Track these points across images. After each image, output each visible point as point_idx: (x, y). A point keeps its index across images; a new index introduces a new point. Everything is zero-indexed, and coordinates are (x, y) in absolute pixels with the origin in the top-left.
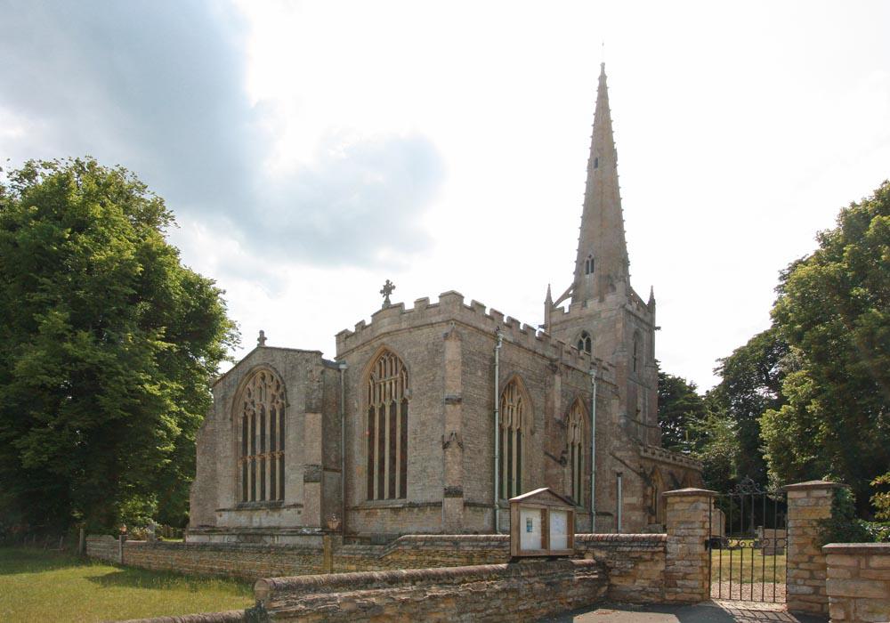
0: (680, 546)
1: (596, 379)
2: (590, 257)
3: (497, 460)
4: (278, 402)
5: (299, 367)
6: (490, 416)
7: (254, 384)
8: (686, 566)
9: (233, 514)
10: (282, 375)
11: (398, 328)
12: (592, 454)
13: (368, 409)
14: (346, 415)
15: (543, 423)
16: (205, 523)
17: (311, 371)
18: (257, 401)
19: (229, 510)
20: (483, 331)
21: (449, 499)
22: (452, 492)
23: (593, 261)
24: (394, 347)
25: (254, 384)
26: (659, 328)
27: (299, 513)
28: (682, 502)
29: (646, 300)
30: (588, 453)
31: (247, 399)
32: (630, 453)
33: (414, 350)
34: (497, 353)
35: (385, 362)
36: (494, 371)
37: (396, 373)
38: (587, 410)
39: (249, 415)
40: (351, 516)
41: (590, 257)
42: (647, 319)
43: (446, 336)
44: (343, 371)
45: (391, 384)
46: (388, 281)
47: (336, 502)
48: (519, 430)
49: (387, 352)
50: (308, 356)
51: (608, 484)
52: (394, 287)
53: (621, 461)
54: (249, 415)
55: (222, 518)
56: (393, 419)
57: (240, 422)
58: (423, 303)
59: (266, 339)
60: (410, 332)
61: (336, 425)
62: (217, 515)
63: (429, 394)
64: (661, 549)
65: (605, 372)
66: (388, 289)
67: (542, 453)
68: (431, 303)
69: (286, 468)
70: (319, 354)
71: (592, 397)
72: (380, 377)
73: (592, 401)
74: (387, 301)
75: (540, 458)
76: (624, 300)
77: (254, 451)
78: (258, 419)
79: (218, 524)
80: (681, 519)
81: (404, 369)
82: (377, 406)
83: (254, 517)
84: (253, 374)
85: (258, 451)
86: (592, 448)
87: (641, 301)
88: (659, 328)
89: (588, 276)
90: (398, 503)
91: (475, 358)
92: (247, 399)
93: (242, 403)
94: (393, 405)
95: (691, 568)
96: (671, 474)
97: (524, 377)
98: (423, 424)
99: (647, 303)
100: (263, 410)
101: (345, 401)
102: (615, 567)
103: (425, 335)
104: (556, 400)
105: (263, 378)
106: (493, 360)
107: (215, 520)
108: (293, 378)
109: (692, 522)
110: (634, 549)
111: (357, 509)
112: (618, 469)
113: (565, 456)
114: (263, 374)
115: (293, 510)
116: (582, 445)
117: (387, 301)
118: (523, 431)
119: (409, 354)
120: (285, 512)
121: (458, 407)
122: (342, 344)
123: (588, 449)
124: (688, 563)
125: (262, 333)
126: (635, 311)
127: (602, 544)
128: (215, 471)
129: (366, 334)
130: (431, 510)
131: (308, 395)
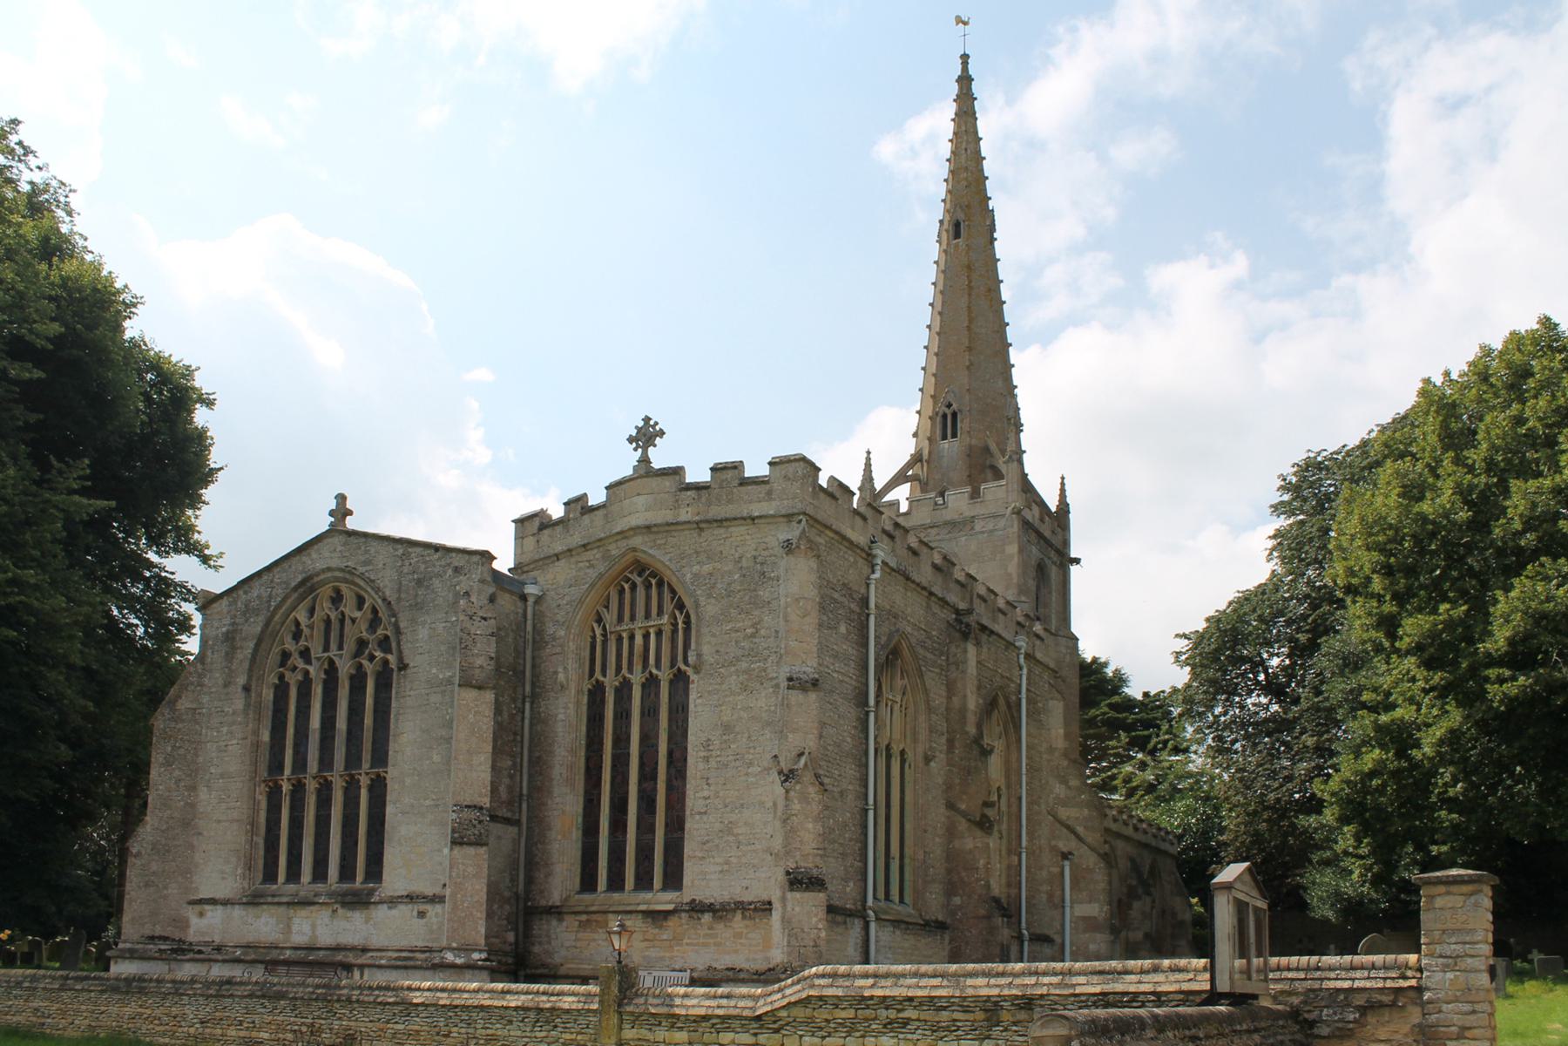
0: (1450, 975)
1: (1028, 656)
2: (949, 405)
3: (871, 814)
4: (372, 658)
5: (436, 583)
6: (859, 719)
7: (312, 611)
8: (1466, 1014)
9: (237, 912)
10: (392, 598)
11: (670, 519)
12: (1020, 811)
13: (587, 686)
14: (534, 697)
15: (943, 740)
16: (158, 931)
17: (467, 594)
18: (316, 651)
19: (225, 903)
20: (851, 542)
21: (798, 895)
22: (799, 881)
23: (954, 415)
24: (661, 555)
25: (312, 611)
26: (1077, 561)
27: (422, 914)
28: (1448, 893)
29: (1053, 504)
30: (1014, 809)
31: (290, 645)
32: (1086, 812)
33: (707, 568)
34: (872, 587)
35: (634, 587)
36: (867, 627)
37: (660, 613)
38: (1012, 717)
39: (293, 679)
40: (541, 927)
41: (949, 405)
42: (1056, 541)
43: (788, 547)
44: (531, 600)
45: (646, 636)
46: (647, 419)
47: (507, 894)
48: (903, 753)
49: (641, 568)
50: (458, 561)
51: (1044, 873)
52: (661, 433)
53: (1068, 827)
54: (293, 679)
55: (204, 922)
56: (650, 712)
57: (268, 695)
58: (727, 472)
59: (350, 513)
60: (701, 530)
61: (512, 716)
62: (191, 914)
63: (744, 665)
64: (1413, 982)
65: (1038, 642)
66: (646, 435)
67: (942, 809)
68: (747, 475)
69: (389, 810)
70: (487, 557)
71: (1020, 692)
72: (620, 619)
73: (1020, 699)
74: (644, 460)
75: (938, 815)
76: (1017, 501)
77: (300, 764)
78: (318, 691)
79: (192, 936)
80: (1449, 925)
81: (680, 606)
82: (610, 682)
83: (296, 921)
84: (312, 589)
85: (313, 765)
86: (1020, 799)
87: (1042, 504)
88: (1077, 561)
89: (945, 444)
90: (663, 900)
91: (836, 595)
92: (290, 645)
93: (276, 650)
94: (651, 683)
95: (1472, 1017)
96: (1132, 860)
97: (913, 641)
98: (727, 728)
99: (1053, 509)
100: (331, 671)
101: (534, 666)
102: (1322, 1021)
103: (742, 541)
104: (969, 694)
105: (337, 599)
106: (865, 601)
107: (184, 924)
108: (418, 606)
109: (1472, 931)
110: (1357, 984)
111: (556, 912)
112: (1063, 846)
113: (991, 813)
114: (338, 591)
115: (405, 910)
116: (1003, 787)
117: (644, 460)
118: (910, 755)
119: (696, 576)
120: (381, 912)
121: (813, 696)
122: (530, 542)
123: (1013, 800)
124: (1467, 1007)
125: (341, 498)
126: (1037, 523)
127: (1291, 975)
128: (193, 806)
129: (593, 528)
130: (744, 917)
131: (463, 645)
